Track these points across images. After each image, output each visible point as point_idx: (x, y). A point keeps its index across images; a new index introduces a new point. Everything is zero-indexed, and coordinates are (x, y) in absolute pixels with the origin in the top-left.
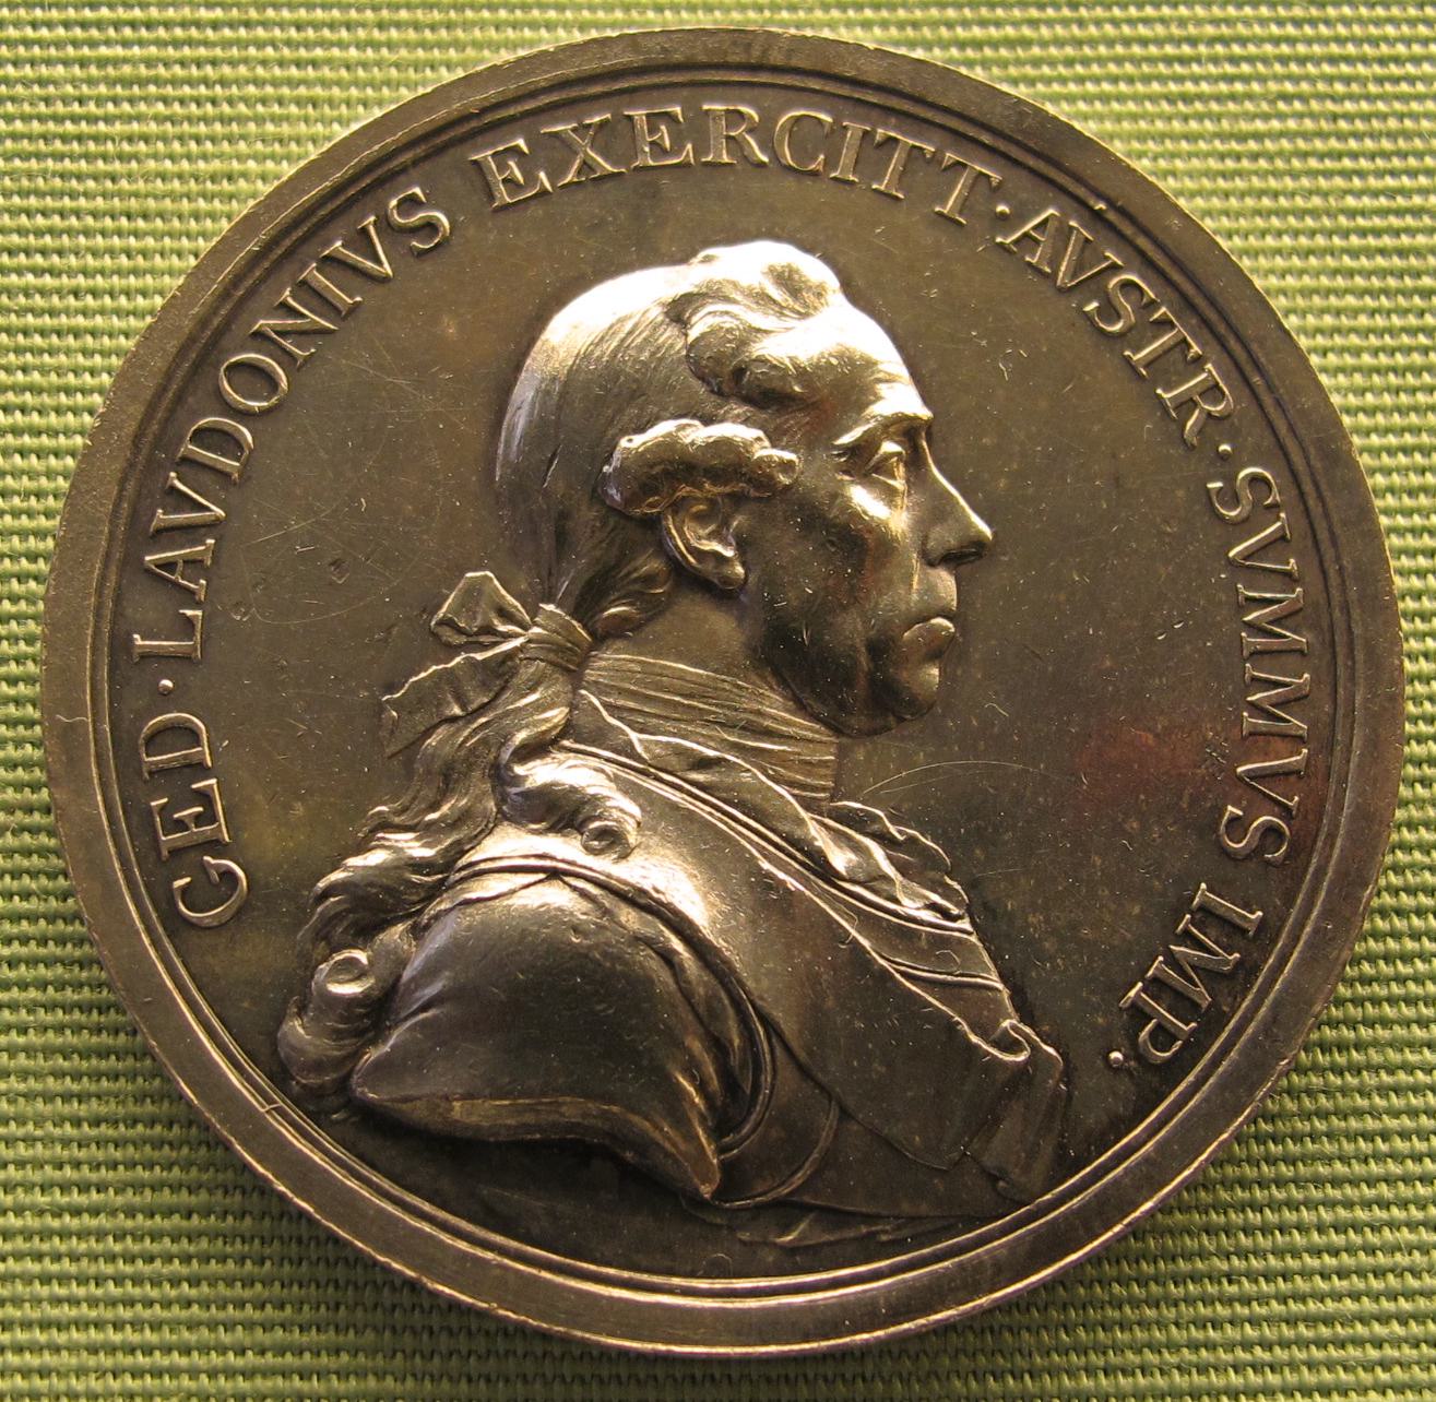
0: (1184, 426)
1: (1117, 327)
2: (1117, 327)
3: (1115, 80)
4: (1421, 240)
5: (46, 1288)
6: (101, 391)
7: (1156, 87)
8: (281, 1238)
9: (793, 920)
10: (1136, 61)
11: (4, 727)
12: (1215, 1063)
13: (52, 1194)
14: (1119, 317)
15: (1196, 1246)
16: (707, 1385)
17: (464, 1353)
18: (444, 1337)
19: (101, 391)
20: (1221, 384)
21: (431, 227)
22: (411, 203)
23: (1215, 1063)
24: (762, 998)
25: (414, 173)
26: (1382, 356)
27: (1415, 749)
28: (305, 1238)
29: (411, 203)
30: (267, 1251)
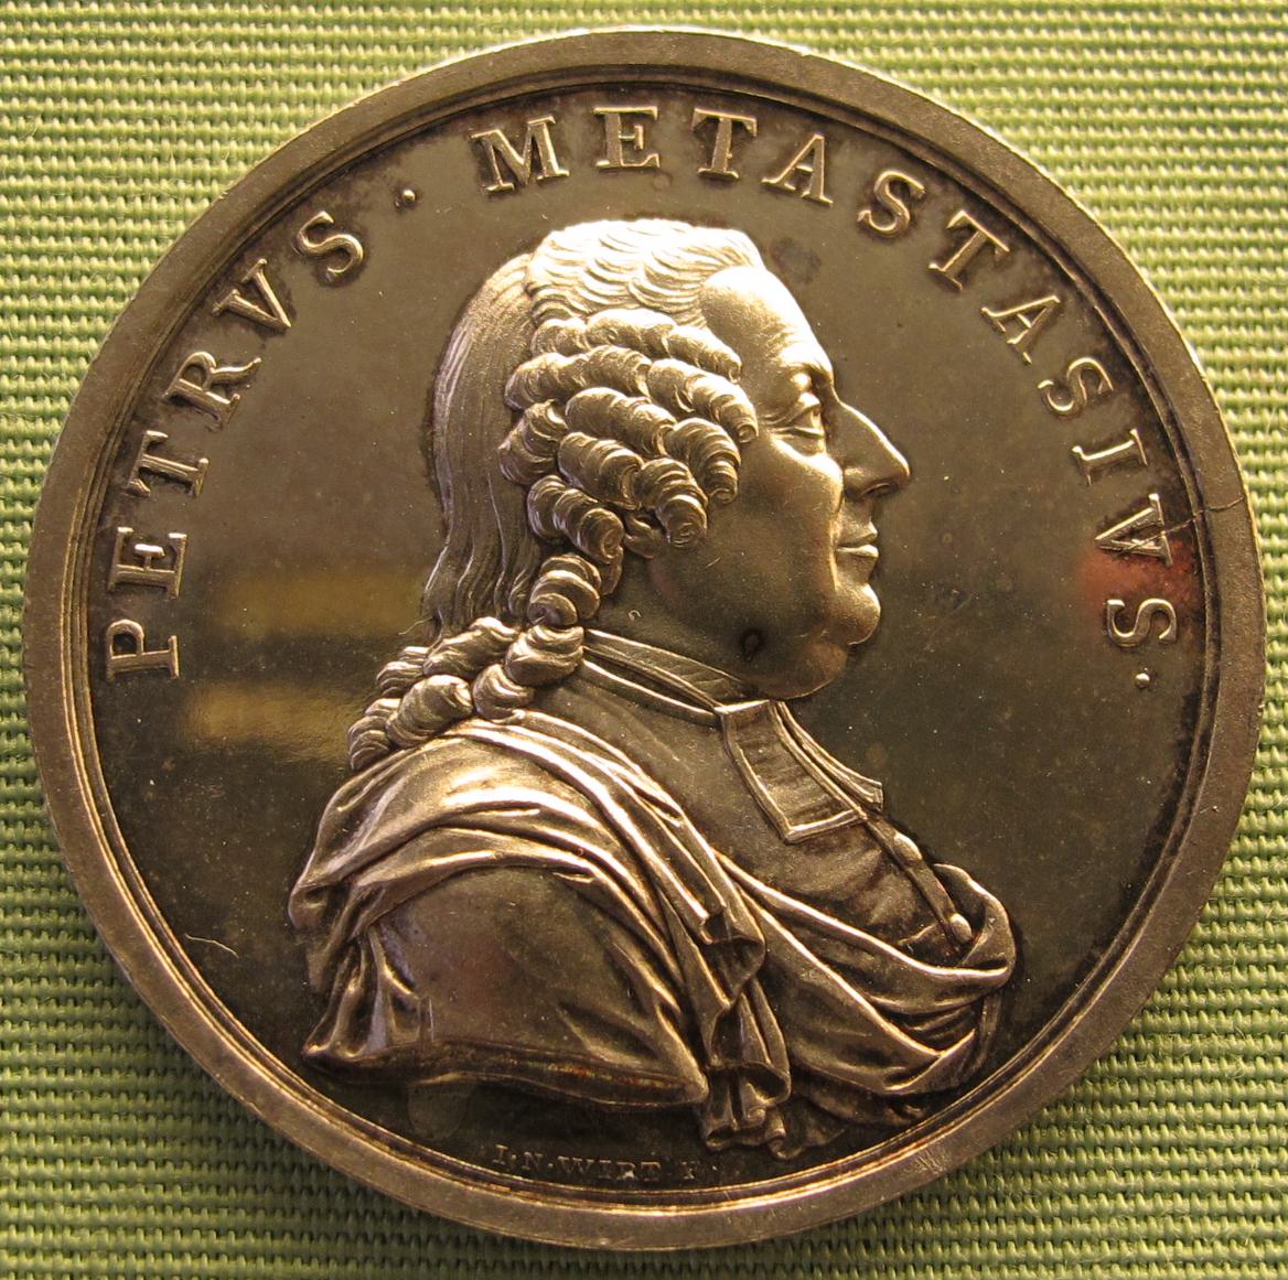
0: (1069, 363)
1: (890, 228)
2: (890, 228)
3: (1214, 145)
4: (1278, 865)
5: (233, 1263)
6: (43, 459)
7: (1115, 75)
8: (255, 1187)
9: (807, 869)
10: (1122, 68)
11: (3, 461)
12: (72, 728)
13: (154, 1190)
14: (892, 220)
15: (1133, 1047)
16: (470, 1247)
17: (434, 1261)
18: (394, 1244)
19: (43, 459)
20: (629, 109)
21: (342, 252)
22: (318, 231)
23: (72, 728)
24: (838, 947)
25: (318, 198)
26: (1175, 231)
27: (1274, 712)
28: (315, 1188)
29: (318, 231)
30: (223, 1199)
